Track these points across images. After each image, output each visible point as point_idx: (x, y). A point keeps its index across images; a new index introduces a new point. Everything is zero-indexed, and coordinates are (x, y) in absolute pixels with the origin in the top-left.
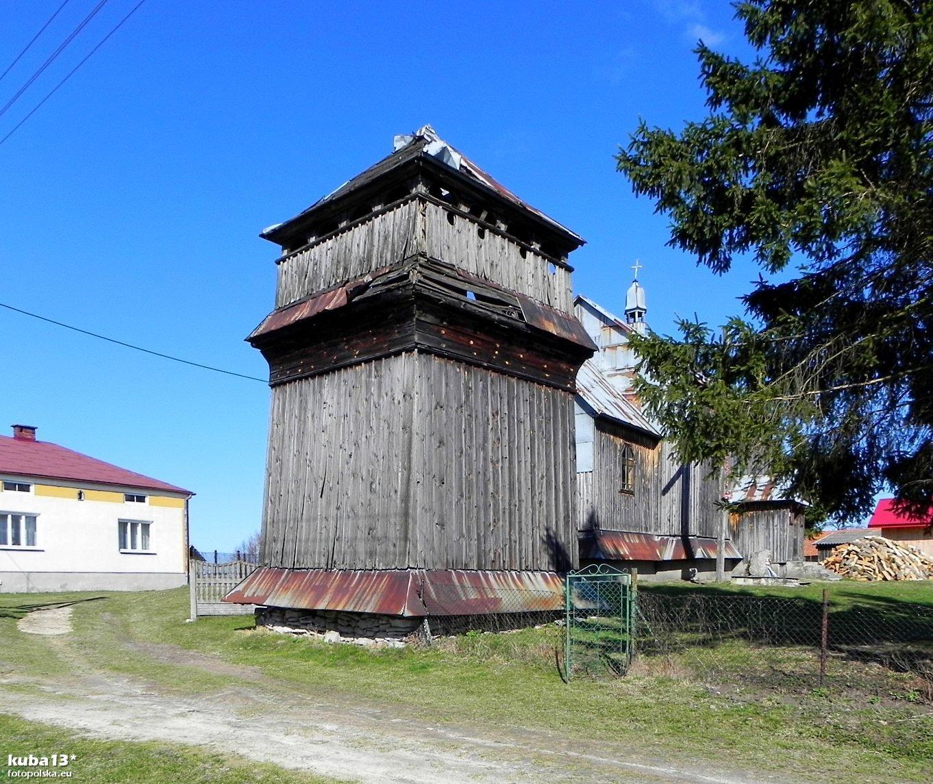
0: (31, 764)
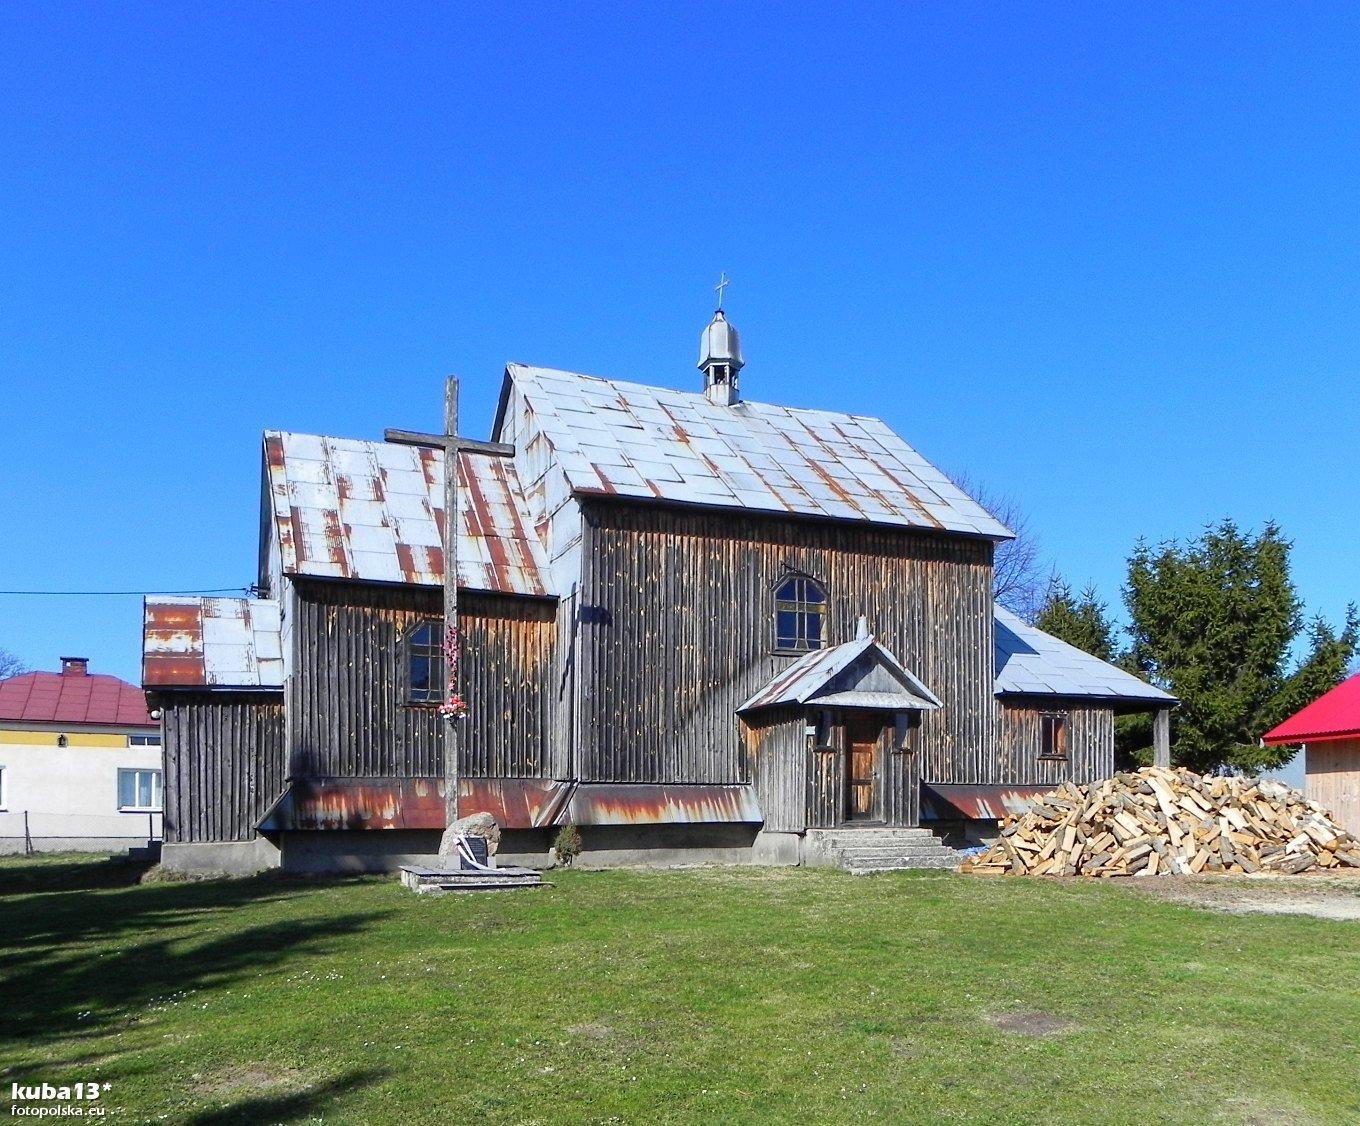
0: (45, 1096)
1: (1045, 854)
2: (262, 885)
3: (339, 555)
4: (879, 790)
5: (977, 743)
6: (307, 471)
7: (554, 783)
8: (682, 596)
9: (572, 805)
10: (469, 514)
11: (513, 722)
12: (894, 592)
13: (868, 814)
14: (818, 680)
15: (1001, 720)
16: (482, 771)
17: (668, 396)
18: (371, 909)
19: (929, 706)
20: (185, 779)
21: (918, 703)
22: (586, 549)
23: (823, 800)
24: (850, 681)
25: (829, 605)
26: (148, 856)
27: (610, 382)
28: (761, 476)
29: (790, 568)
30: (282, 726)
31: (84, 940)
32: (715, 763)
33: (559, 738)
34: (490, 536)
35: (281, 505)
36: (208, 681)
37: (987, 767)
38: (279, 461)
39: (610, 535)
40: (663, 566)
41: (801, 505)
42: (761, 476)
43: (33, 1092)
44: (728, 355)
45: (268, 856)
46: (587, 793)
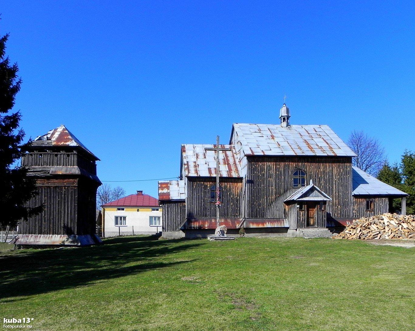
1: (353, 234)
2: (182, 239)
3: (196, 171)
4: (316, 219)
5: (347, 207)
6: (189, 156)
7: (242, 219)
8: (270, 176)
9: (245, 223)
10: (224, 159)
11: (233, 205)
12: (324, 172)
13: (313, 225)
14: (300, 195)
15: (354, 202)
16: (226, 216)
17: (271, 126)
18: (203, 243)
19: (328, 200)
20: (166, 219)
21: (325, 199)
22: (248, 167)
23: (301, 222)
24: (308, 195)
25: (307, 176)
26: (160, 234)
27: (257, 125)
28: (291, 146)
29: (297, 168)
30: (185, 207)
32: (277, 214)
33: (243, 209)
34: (228, 164)
35: (185, 161)
36: (171, 199)
37: (350, 214)
38: (184, 151)
39: (253, 164)
40: (266, 170)
41: (299, 153)
42: (291, 146)
43: (10, 321)
44: (286, 115)
45: (182, 235)
46: (248, 221)
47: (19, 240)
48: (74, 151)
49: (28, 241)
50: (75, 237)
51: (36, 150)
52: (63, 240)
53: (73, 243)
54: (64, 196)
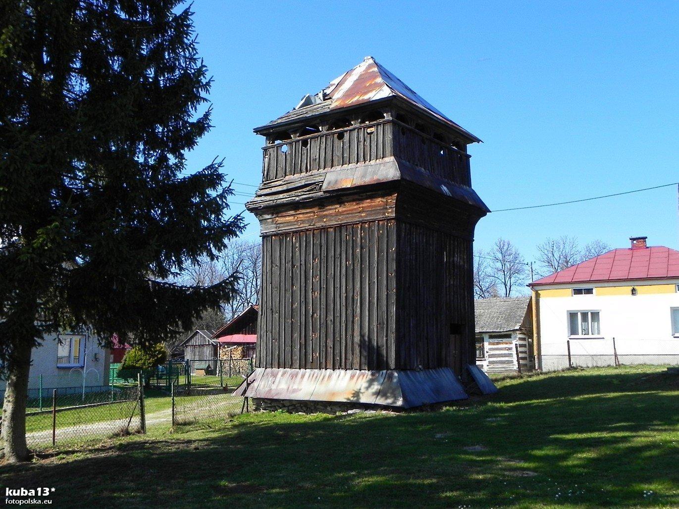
31: (648, 430)
43: (16, 492)
47: (255, 384)
48: (385, 115)
49: (274, 387)
50: (390, 377)
51: (295, 132)
52: (357, 388)
53: (382, 396)
54: (361, 251)
